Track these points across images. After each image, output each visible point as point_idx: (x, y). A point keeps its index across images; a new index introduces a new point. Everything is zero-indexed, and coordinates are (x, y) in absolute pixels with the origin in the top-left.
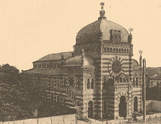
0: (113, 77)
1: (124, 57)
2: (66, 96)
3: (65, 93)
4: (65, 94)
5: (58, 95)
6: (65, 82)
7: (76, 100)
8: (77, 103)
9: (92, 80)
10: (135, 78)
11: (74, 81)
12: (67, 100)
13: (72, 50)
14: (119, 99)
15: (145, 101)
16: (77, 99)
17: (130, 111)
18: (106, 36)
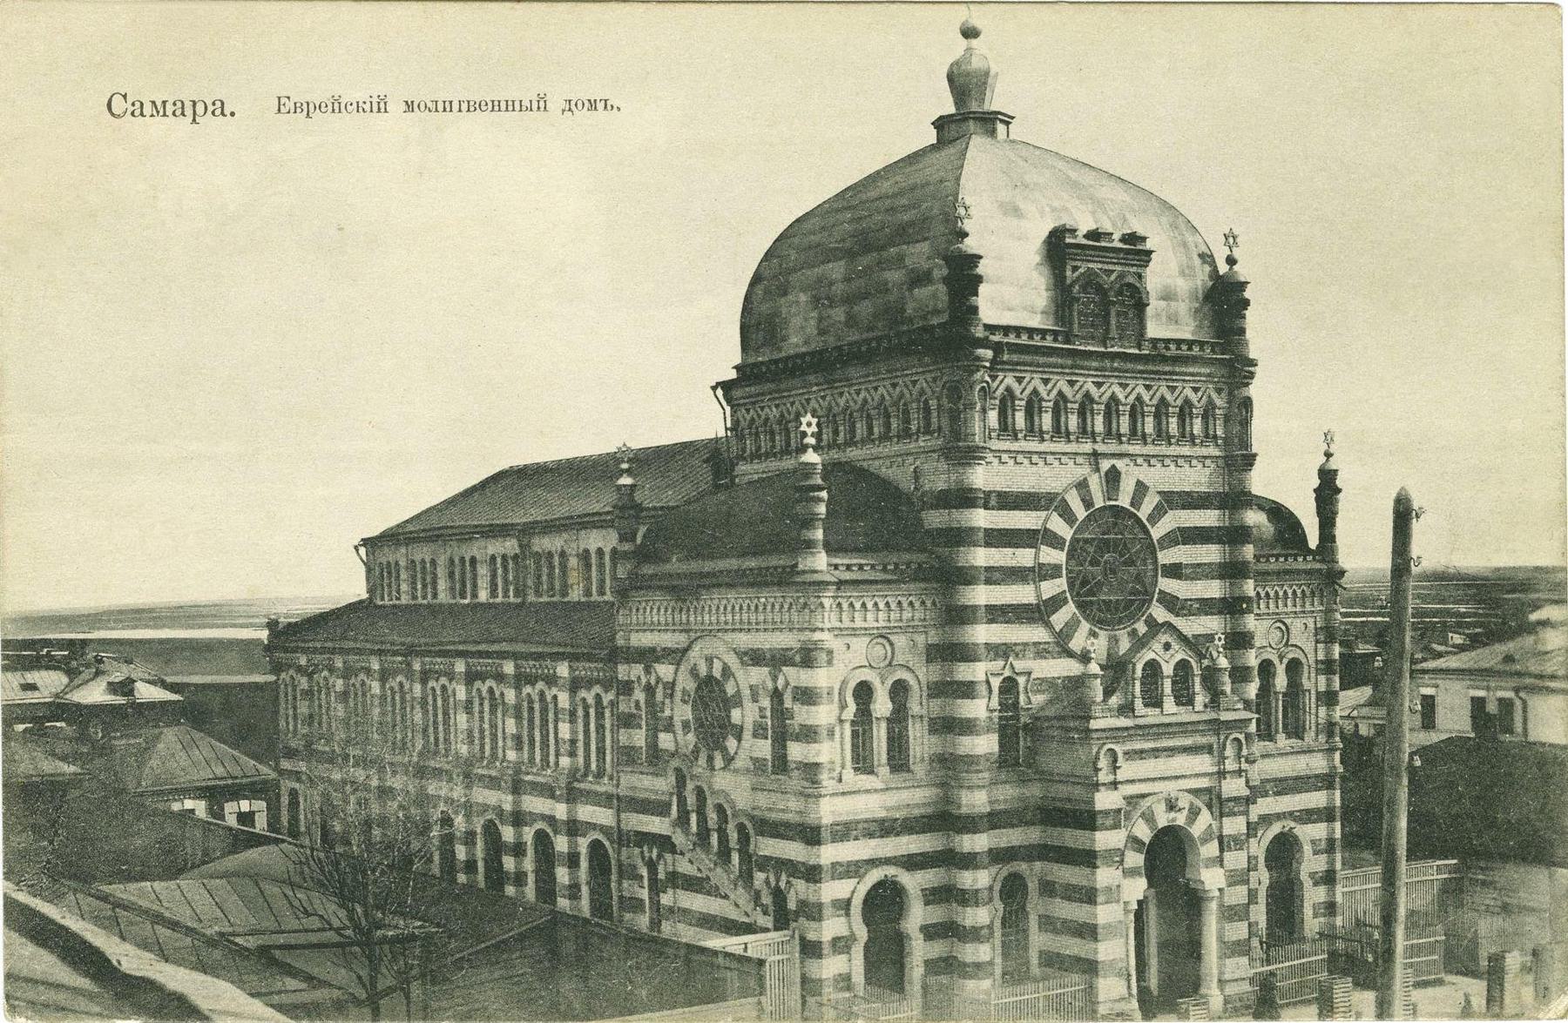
0: (1085, 658)
1: (1170, 472)
2: (665, 843)
3: (660, 809)
4: (656, 825)
5: (540, 825)
6: (660, 724)
7: (759, 877)
8: (767, 899)
9: (899, 691)
10: (1281, 670)
11: (739, 704)
12: (675, 880)
13: (708, 421)
14: (1135, 859)
15: (1403, 865)
16: (766, 863)
17: (796, 321)
18: (1013, 293)
